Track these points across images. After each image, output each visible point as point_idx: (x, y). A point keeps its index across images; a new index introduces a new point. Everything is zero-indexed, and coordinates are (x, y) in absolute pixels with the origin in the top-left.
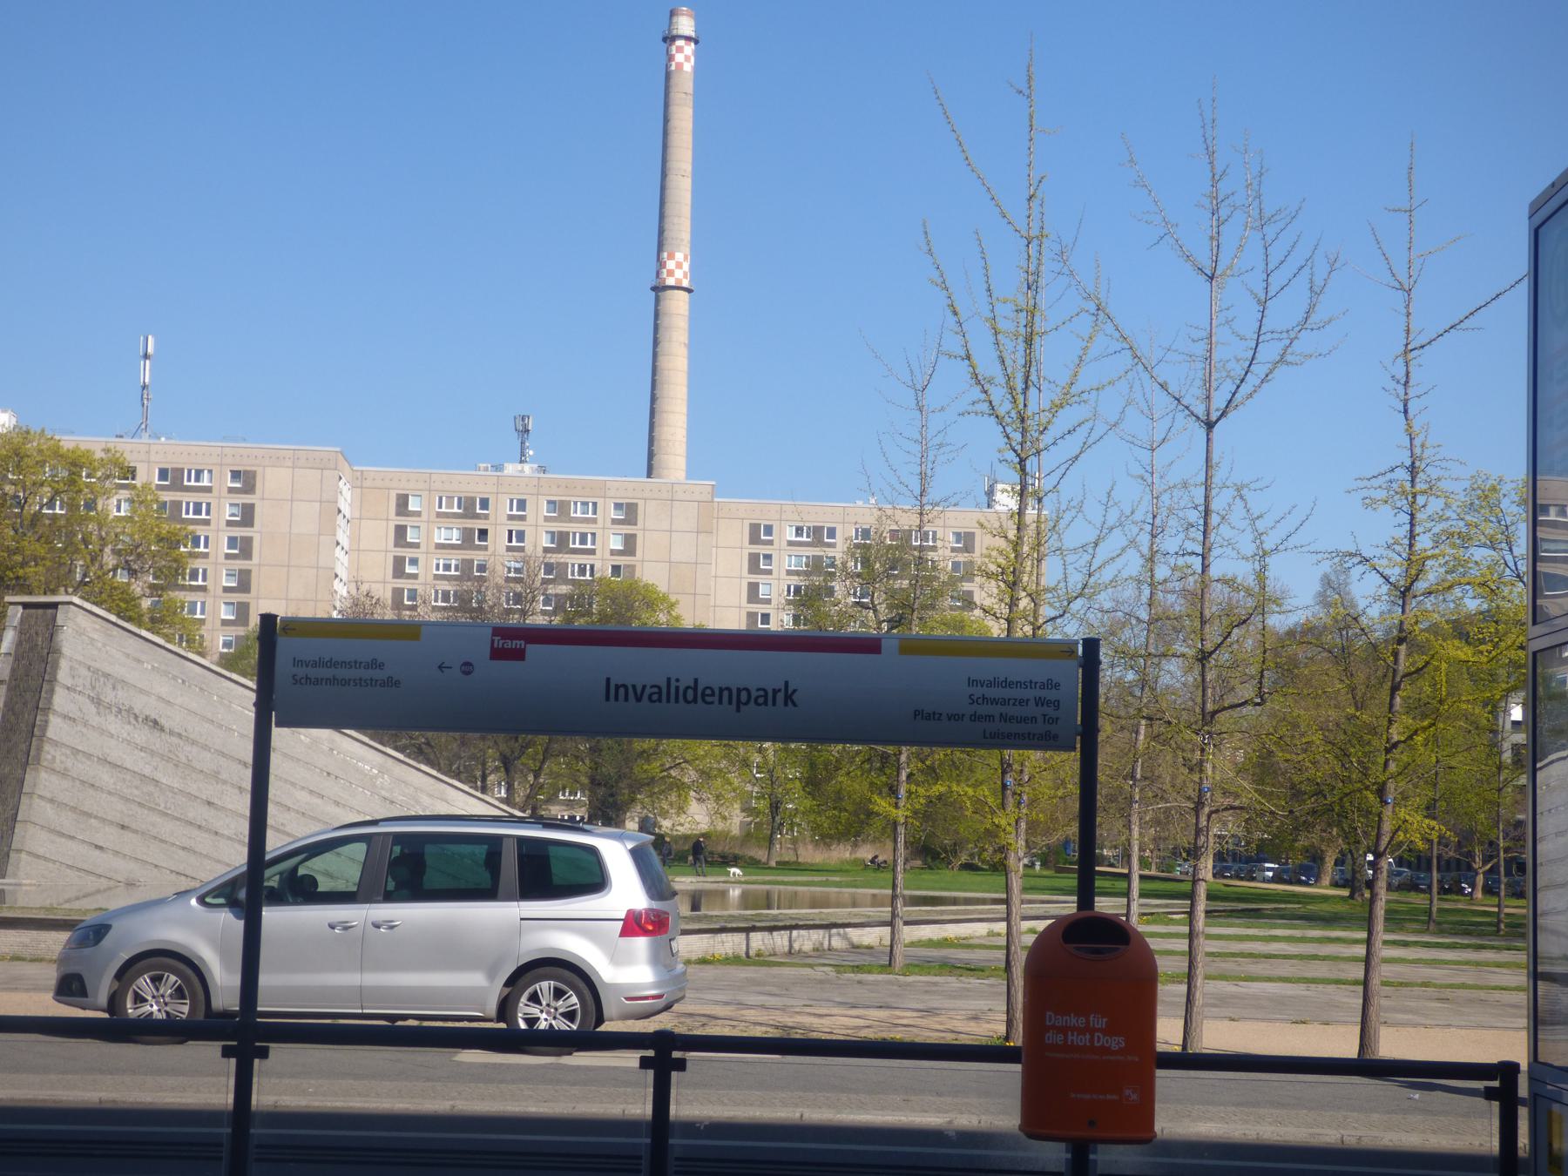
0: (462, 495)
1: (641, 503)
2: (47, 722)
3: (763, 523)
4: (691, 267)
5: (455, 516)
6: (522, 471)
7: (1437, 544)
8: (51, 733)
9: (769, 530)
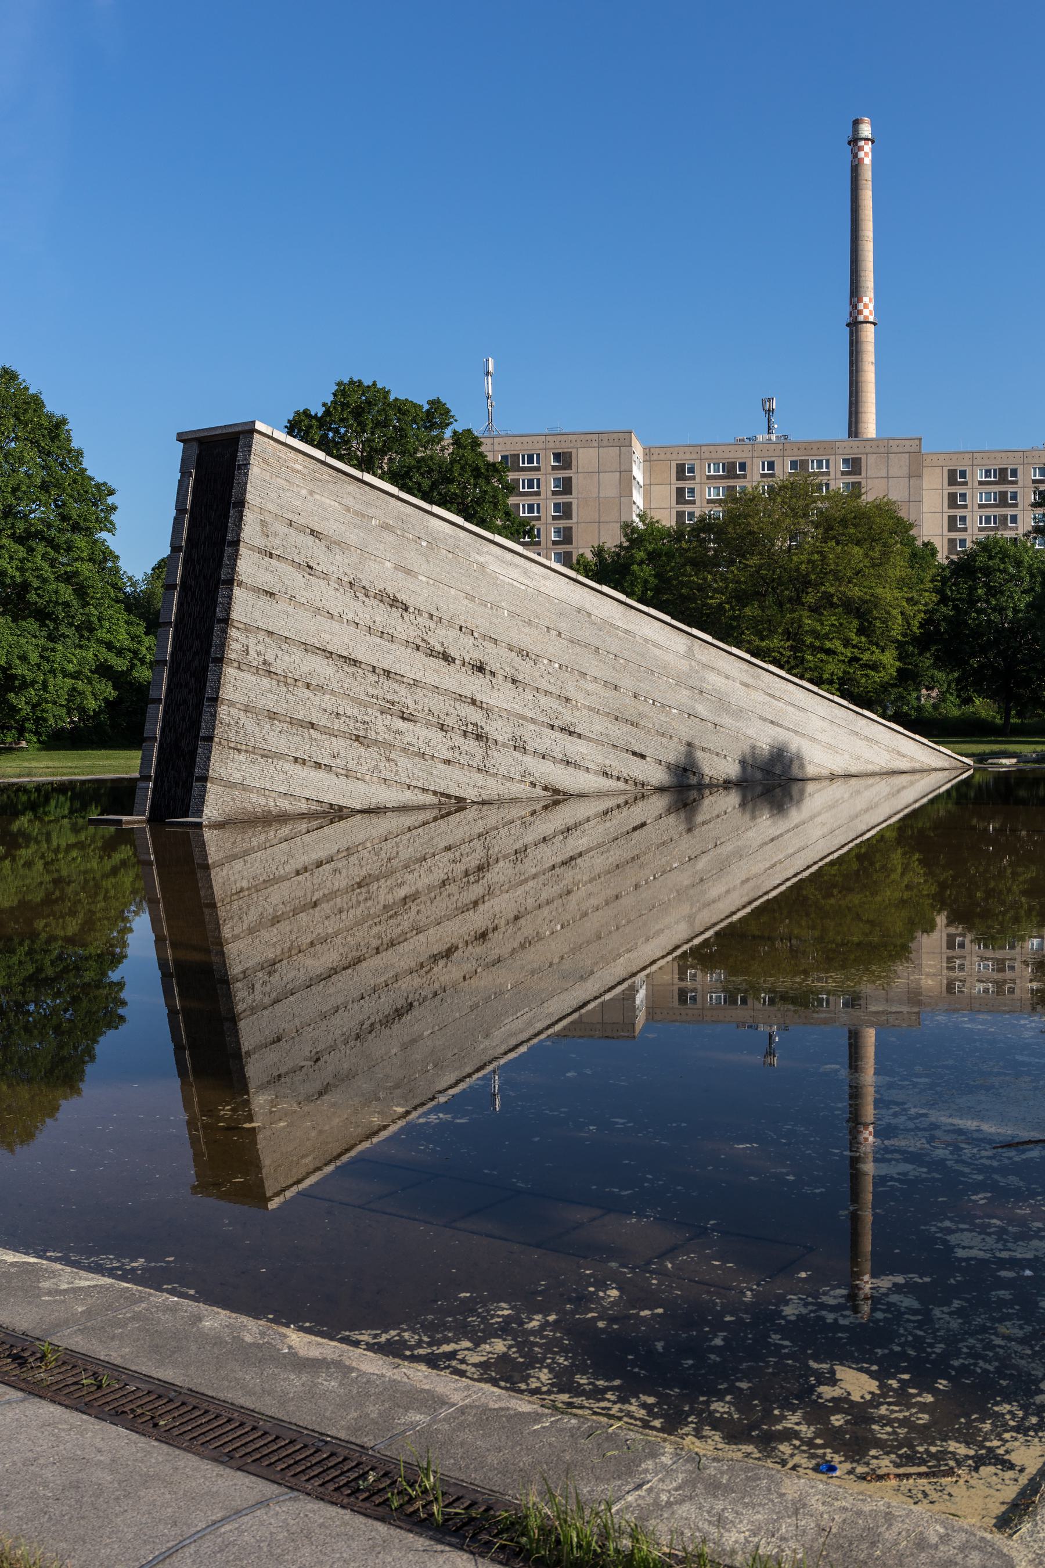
0: (726, 461)
1: (863, 457)
2: (230, 597)
3: (959, 469)
6: (770, 439)
8: (237, 613)
9: (963, 474)
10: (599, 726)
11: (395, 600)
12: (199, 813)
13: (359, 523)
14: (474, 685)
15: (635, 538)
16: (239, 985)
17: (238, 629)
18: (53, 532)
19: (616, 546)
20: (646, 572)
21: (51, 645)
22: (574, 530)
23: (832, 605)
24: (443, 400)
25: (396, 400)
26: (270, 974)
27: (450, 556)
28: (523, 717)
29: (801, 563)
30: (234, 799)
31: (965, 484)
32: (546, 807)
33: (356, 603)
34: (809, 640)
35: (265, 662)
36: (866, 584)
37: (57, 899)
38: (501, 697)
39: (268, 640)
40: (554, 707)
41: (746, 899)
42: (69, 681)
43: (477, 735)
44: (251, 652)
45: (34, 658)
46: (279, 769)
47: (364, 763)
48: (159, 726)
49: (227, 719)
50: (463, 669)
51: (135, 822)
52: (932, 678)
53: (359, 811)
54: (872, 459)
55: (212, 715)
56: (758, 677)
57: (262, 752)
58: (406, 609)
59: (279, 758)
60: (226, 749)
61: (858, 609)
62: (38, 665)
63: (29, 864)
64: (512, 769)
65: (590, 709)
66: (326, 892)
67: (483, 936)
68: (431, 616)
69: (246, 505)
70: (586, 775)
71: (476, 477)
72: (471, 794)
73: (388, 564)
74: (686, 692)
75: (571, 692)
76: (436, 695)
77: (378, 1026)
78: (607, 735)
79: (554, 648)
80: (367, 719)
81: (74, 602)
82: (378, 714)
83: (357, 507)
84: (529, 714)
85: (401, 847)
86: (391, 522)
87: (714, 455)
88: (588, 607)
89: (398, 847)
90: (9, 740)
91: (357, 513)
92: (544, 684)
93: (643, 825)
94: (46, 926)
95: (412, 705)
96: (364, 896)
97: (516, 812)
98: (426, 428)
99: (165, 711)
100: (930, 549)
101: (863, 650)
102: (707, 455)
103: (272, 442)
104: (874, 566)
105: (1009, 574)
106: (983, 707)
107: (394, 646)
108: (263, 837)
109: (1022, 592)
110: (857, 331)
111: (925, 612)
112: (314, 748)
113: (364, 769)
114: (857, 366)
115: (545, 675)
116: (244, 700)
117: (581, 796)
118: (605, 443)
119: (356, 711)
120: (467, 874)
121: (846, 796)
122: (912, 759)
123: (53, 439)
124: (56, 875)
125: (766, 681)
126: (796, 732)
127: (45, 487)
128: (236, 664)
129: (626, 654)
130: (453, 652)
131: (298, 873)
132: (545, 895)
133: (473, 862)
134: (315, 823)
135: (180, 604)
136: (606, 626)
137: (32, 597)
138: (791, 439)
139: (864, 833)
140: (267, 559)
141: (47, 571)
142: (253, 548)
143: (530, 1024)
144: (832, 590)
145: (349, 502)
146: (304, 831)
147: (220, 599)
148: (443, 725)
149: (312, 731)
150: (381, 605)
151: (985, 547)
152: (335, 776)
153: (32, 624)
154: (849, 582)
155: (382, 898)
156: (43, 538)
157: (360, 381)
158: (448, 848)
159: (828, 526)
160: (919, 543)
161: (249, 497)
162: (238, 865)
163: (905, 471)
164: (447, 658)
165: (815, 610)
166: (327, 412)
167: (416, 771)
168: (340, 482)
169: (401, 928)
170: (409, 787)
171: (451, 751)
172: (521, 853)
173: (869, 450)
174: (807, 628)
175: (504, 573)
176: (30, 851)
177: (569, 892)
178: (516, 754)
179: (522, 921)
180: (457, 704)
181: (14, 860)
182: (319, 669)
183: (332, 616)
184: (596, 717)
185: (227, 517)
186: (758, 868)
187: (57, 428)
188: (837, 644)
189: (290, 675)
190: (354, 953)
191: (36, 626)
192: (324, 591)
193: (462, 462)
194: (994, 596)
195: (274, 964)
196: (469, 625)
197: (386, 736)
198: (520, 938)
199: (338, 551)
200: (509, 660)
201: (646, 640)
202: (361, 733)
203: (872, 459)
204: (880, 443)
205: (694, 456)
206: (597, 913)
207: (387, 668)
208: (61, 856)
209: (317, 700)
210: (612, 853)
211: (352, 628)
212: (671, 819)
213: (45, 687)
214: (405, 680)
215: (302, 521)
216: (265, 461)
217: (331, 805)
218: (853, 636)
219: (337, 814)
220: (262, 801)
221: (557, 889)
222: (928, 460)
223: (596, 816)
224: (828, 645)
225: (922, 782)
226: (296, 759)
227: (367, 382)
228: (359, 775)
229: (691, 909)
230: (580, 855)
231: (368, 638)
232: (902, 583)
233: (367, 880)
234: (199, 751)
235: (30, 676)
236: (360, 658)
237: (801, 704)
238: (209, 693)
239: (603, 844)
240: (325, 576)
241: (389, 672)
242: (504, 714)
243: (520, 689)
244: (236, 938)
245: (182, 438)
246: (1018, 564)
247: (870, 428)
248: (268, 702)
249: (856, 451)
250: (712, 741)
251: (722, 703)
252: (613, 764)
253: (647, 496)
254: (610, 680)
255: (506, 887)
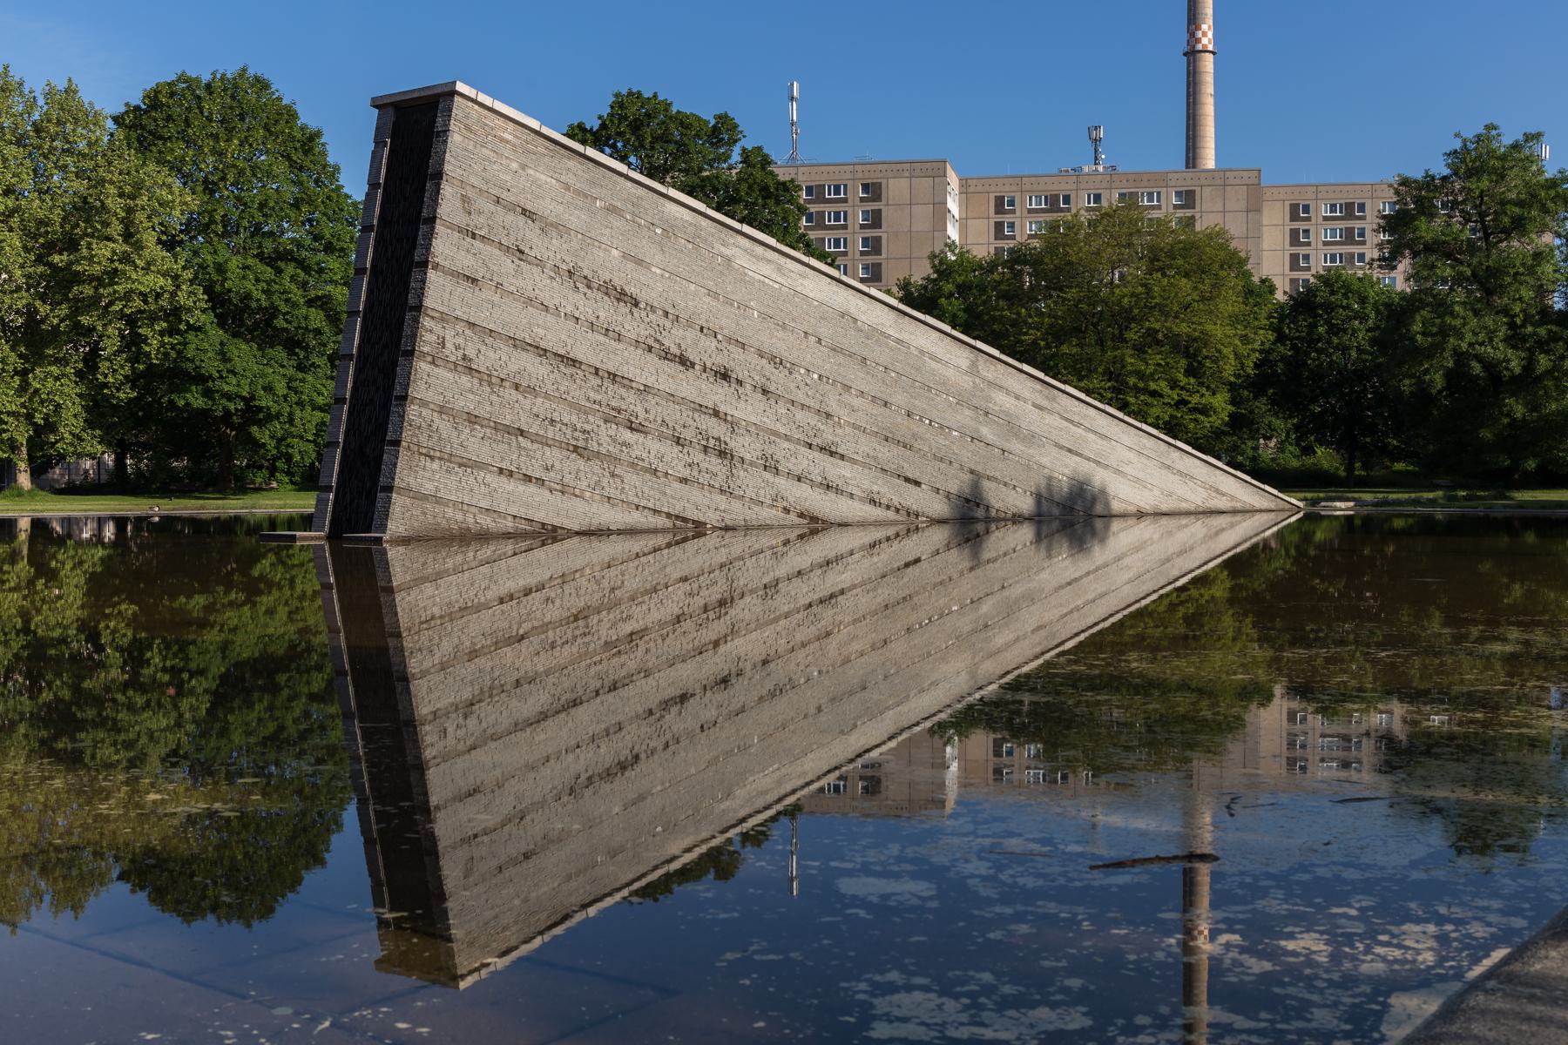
1: (1198, 189)
2: (423, 281)
3: (1302, 203)
4: (1214, 35)
5: (1043, 211)
7: (95, 821)
9: (1306, 209)
10: (865, 446)
11: (623, 293)
12: (383, 528)
13: (580, 203)
14: (718, 395)
15: (944, 270)
16: (427, 728)
17: (433, 318)
18: (304, 253)
19: (923, 279)
20: (956, 305)
21: (300, 375)
22: (883, 267)
23: (1158, 343)
24: (731, 115)
25: (678, 112)
26: (466, 717)
27: (690, 246)
28: (776, 434)
29: (1123, 297)
30: (425, 514)
31: (1309, 219)
32: (801, 537)
33: (575, 295)
34: (1132, 381)
35: (464, 357)
36: (1195, 319)
37: (304, 651)
38: (748, 409)
39: (467, 332)
40: (812, 423)
41: (1038, 650)
42: (318, 414)
43: (720, 451)
44: (447, 345)
45: (281, 388)
46: (480, 480)
47: (583, 478)
48: (343, 428)
49: (418, 421)
50: (704, 375)
51: (312, 538)
52: (1269, 426)
53: (578, 533)
54: (1207, 191)
55: (400, 416)
56: (1054, 399)
57: (459, 460)
58: (636, 304)
59: (481, 468)
60: (417, 456)
61: (1187, 348)
62: (285, 397)
63: (271, 612)
64: (762, 492)
65: (855, 426)
66: (536, 624)
67: (725, 681)
68: (666, 314)
69: (445, 177)
70: (850, 502)
71: (765, 198)
72: (711, 518)
73: (615, 253)
74: (968, 412)
75: (833, 406)
76: (671, 404)
77: (596, 779)
78: (875, 458)
79: (812, 355)
80: (588, 427)
81: (326, 329)
82: (601, 423)
83: (578, 186)
84: (782, 430)
85: (627, 577)
86: (619, 205)
87: (1035, 187)
88: (853, 311)
89: (623, 575)
90: (259, 480)
91: (578, 193)
92: (800, 397)
93: (917, 561)
94: (288, 680)
95: (642, 415)
96: (582, 631)
97: (765, 540)
98: (712, 144)
99: (350, 413)
100: (1268, 286)
101: (1191, 393)
102: (1028, 187)
103: (476, 107)
104: (1203, 299)
105: (1353, 310)
106: (1325, 457)
107: (621, 346)
108: (459, 558)
109: (1367, 331)
110: (1195, 61)
111: (1261, 352)
112: (522, 459)
113: (583, 484)
114: (1194, 98)
115: (802, 385)
116: (439, 399)
117: (843, 525)
118: (918, 172)
119: (574, 418)
120: (706, 609)
121: (1156, 537)
122: (1233, 498)
123: (306, 153)
124: (301, 625)
125: (1063, 403)
126: (1098, 463)
127: (296, 205)
128: (429, 359)
129: (898, 367)
130: (692, 355)
131: (501, 601)
132: (799, 637)
133: (714, 595)
134: (524, 545)
135: (370, 291)
136: (875, 334)
137: (280, 322)
138: (1120, 169)
139: (1176, 580)
140: (469, 240)
141: (297, 295)
142: (451, 226)
143: (779, 782)
144: (1157, 326)
145: (570, 179)
146: (510, 553)
147: (412, 284)
148: (679, 438)
149: (520, 439)
150: (606, 298)
151: (1326, 280)
152: (548, 492)
153: (279, 353)
154: (1176, 317)
155: (603, 633)
156: (294, 259)
157: (639, 93)
158: (685, 579)
159: (1157, 260)
160: (1256, 279)
161: (447, 167)
162: (429, 589)
163: (1242, 205)
164: (684, 362)
165: (1140, 350)
166: (603, 126)
167: (646, 490)
168: (558, 156)
169: (625, 668)
170: (637, 507)
171: (689, 469)
172: (771, 587)
173: (1203, 182)
174: (1129, 368)
175: (754, 268)
176: (271, 598)
177: (828, 634)
178: (767, 475)
179: (772, 665)
180: (696, 415)
181: (254, 604)
182: (530, 368)
183: (547, 308)
184: (863, 438)
185: (423, 190)
186: (1052, 615)
187: (310, 141)
188: (1162, 386)
189: (496, 373)
190: (568, 695)
191: (284, 354)
192: (538, 279)
193: (750, 181)
194: (1336, 334)
195: (472, 704)
196: (711, 325)
197: (611, 449)
198: (769, 685)
199: (554, 234)
200: (758, 368)
201: (922, 352)
202: (581, 444)
203: (1207, 191)
204: (1216, 174)
205: (1014, 188)
206: (862, 659)
207: (612, 370)
208: (306, 604)
209: (527, 403)
210: (880, 591)
211: (571, 323)
212: (954, 554)
213: (291, 421)
214: (634, 385)
215: (511, 198)
216: (468, 128)
217: (543, 524)
218: (1181, 377)
219: (550, 534)
220: (459, 517)
221: (813, 631)
222: (1269, 194)
223: (862, 548)
224: (1153, 386)
225: (1245, 525)
226: (501, 471)
227: (647, 94)
228: (577, 492)
229: (974, 657)
230: (842, 592)
231: (590, 335)
232: (1235, 320)
233: (586, 613)
234: (385, 457)
235: (275, 408)
236: (580, 357)
237: (1104, 431)
238: (398, 391)
239: (870, 581)
240: (540, 263)
241: (615, 375)
242: (752, 429)
243: (772, 401)
244: (424, 673)
245: (378, 104)
246: (1363, 300)
247: (1209, 160)
248: (468, 403)
249: (1190, 183)
250: (998, 469)
251: (1011, 426)
252: (882, 490)
253: (963, 231)
254: (879, 395)
255: (753, 626)
